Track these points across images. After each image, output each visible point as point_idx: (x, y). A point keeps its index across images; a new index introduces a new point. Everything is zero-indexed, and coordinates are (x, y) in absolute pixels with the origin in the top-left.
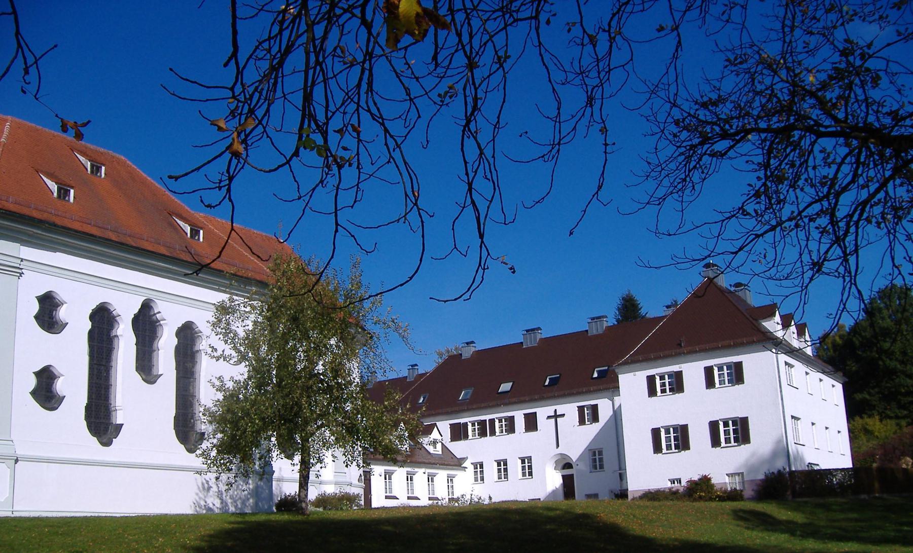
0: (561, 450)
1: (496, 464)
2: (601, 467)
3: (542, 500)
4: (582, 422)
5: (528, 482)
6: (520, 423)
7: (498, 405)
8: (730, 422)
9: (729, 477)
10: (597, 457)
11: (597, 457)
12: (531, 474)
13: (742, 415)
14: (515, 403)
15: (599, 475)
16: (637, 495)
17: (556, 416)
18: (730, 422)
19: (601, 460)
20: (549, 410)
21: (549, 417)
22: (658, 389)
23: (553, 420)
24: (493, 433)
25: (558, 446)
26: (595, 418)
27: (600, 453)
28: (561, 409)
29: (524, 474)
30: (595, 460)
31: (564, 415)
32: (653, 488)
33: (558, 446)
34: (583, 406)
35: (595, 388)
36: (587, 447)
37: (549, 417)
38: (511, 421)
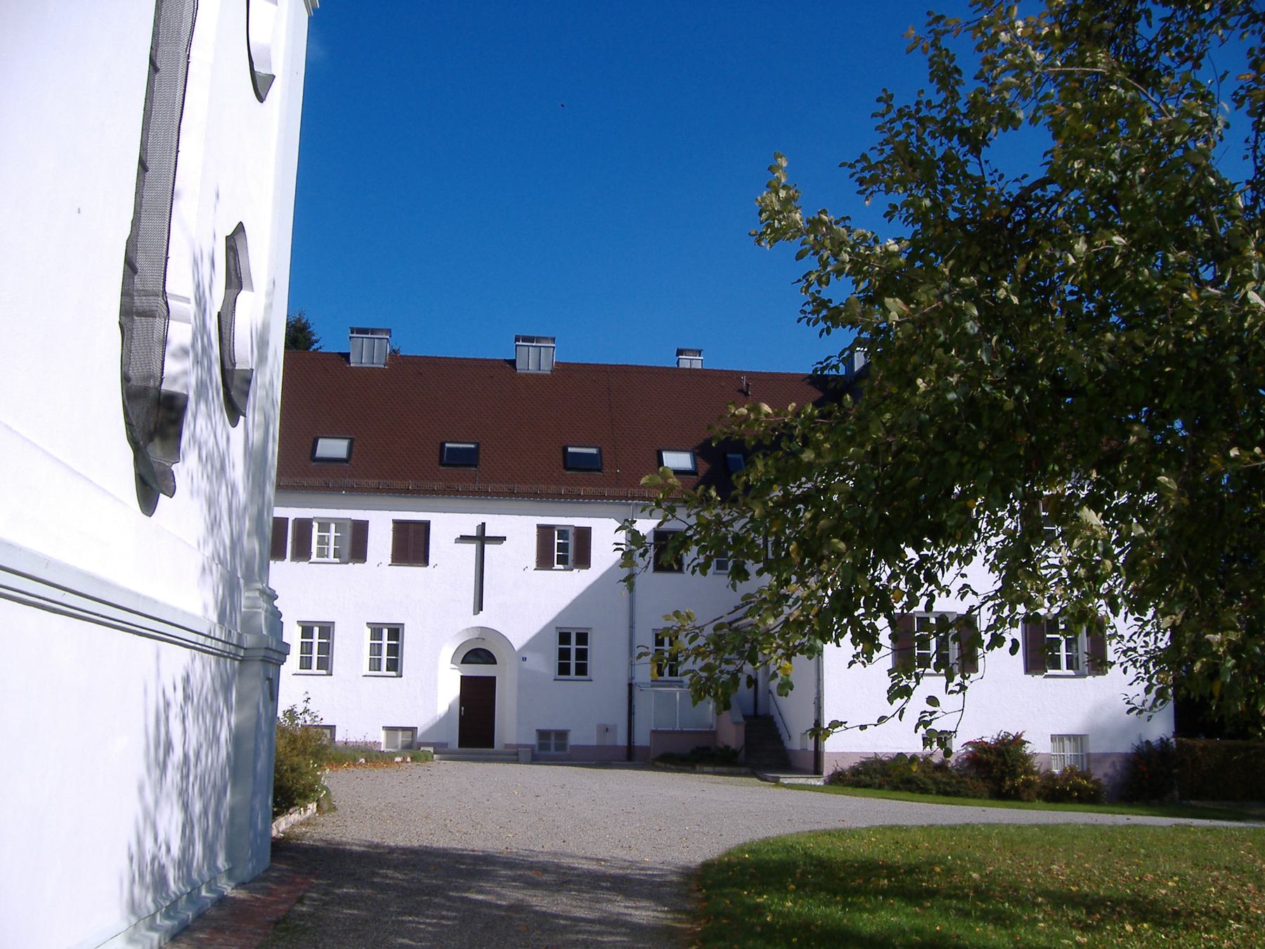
0: (483, 620)
1: (368, 632)
2: (582, 670)
3: (419, 732)
4: (544, 561)
5: (387, 684)
6: (381, 539)
7: (337, 489)
8: (316, 630)
9: (1070, 740)
10: (573, 646)
11: (573, 646)
12: (394, 665)
13: (395, 619)
14: (377, 491)
15: (574, 687)
16: (845, 765)
17: (481, 539)
18: (316, 630)
19: (582, 654)
20: (468, 523)
21: (464, 539)
22: (571, 542)
23: (471, 548)
24: (302, 553)
25: (479, 606)
26: (583, 559)
27: (582, 638)
28: (496, 524)
29: (375, 665)
30: (564, 654)
31: (504, 538)
32: (884, 750)
33: (479, 606)
34: (551, 528)
35: (591, 490)
36: (554, 621)
37: (464, 539)
38: (359, 532)
